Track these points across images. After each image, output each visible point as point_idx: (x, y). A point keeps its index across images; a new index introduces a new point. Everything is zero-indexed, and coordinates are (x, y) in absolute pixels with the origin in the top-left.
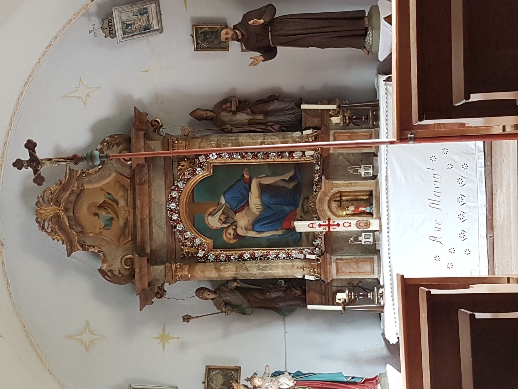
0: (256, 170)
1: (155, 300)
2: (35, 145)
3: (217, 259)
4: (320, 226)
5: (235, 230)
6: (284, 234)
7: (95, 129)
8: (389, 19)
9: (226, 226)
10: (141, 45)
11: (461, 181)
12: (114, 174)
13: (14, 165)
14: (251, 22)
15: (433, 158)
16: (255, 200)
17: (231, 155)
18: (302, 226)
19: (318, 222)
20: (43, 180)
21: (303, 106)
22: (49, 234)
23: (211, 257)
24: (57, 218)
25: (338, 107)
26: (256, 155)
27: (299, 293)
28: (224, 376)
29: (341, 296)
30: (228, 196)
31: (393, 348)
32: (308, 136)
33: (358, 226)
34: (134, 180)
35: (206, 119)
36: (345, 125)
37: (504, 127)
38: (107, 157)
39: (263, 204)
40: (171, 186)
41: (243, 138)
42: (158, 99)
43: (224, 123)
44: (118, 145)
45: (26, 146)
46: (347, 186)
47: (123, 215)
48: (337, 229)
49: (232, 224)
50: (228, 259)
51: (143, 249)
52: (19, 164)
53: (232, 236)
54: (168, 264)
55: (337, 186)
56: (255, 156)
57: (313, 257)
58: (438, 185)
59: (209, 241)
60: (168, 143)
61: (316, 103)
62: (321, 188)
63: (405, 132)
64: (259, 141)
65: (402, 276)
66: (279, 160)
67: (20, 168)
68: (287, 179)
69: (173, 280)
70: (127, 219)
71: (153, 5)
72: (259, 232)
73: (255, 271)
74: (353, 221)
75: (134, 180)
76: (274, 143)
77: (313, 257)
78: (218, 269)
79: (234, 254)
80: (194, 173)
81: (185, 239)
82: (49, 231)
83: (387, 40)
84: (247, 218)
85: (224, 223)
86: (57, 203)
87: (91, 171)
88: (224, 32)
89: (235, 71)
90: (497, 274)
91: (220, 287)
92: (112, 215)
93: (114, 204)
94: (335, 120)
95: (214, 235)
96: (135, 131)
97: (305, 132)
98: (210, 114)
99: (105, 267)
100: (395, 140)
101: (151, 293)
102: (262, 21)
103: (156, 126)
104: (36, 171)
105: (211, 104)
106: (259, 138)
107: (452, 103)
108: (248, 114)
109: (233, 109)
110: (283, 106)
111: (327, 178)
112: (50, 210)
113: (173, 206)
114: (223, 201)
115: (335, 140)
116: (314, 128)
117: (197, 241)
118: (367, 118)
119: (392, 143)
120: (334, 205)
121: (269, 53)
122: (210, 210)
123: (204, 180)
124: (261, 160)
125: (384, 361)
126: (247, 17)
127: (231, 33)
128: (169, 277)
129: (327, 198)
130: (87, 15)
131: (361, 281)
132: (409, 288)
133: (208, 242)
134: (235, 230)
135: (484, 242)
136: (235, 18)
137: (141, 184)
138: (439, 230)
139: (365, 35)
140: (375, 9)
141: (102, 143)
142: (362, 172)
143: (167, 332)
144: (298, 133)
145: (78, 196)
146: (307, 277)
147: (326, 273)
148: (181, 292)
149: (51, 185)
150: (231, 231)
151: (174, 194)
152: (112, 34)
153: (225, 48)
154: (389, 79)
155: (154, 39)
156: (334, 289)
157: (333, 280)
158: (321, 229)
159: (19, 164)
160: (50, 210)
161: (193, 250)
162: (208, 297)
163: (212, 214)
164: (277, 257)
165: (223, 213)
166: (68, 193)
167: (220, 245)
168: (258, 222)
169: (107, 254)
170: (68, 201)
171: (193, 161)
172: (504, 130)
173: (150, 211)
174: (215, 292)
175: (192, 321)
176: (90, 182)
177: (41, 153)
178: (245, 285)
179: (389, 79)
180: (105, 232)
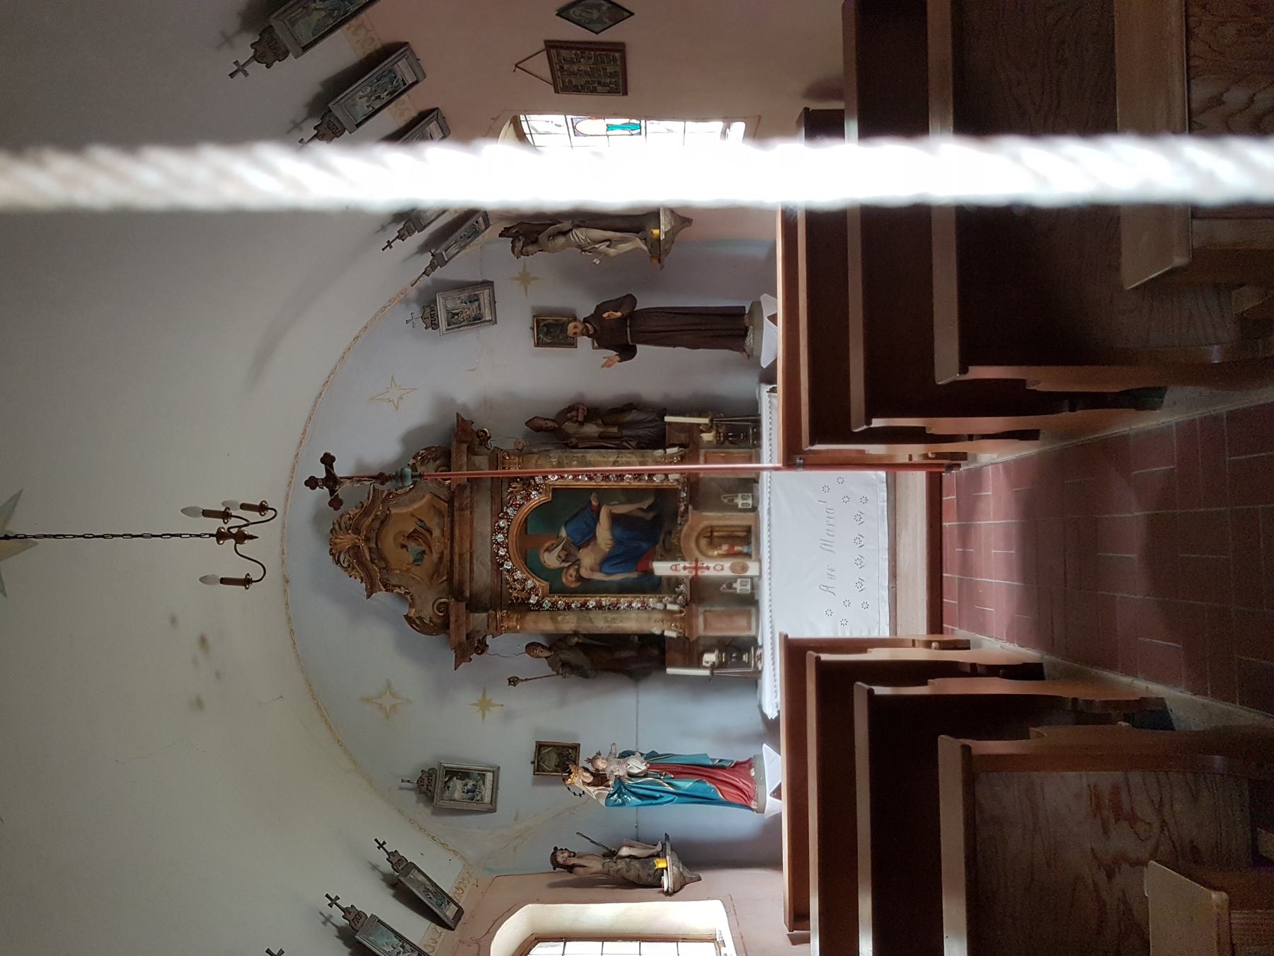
0: (606, 495)
1: (474, 656)
2: (333, 459)
3: (554, 604)
4: (685, 568)
5: (578, 571)
7: (407, 439)
8: (773, 318)
10: (469, 338)
11: (859, 518)
13: (307, 483)
14: (605, 315)
15: (826, 489)
16: (604, 533)
18: (662, 568)
19: (682, 564)
20: (341, 502)
21: (668, 419)
22: (346, 569)
23: (547, 604)
24: (355, 550)
25: (711, 421)
27: (656, 652)
28: (559, 755)
29: (710, 658)
31: (772, 726)
32: (672, 456)
33: (732, 569)
34: (453, 505)
35: (547, 430)
36: (719, 444)
38: (421, 476)
39: (614, 537)
40: (498, 513)
41: (592, 455)
42: (487, 403)
43: (569, 436)
44: (435, 460)
45: (323, 461)
46: (719, 518)
47: (437, 547)
49: (574, 564)
51: (462, 592)
52: (312, 483)
55: (708, 518)
56: (606, 478)
57: (676, 608)
59: (545, 584)
60: (496, 460)
61: (684, 415)
63: (793, 457)
64: (612, 459)
65: (786, 636)
66: (636, 484)
69: (497, 631)
70: (442, 553)
71: (487, 291)
72: (608, 574)
73: (601, 624)
74: (727, 564)
75: (453, 505)
77: (676, 608)
80: (527, 497)
83: (771, 342)
86: (357, 531)
87: (399, 492)
88: (571, 325)
89: (583, 372)
90: (901, 634)
91: (557, 643)
92: (424, 547)
93: (428, 535)
94: (707, 437)
95: (551, 576)
96: (456, 444)
97: (669, 451)
98: (550, 424)
99: (412, 613)
100: (780, 465)
101: (470, 648)
102: (619, 314)
103: (483, 438)
104: (332, 492)
105: (552, 412)
106: (612, 455)
107: (849, 429)
109: (580, 419)
110: (642, 416)
111: (695, 508)
112: (347, 540)
113: (500, 538)
114: (563, 533)
115: (706, 462)
116: (681, 446)
117: (530, 584)
118: (747, 436)
119: (776, 469)
120: (703, 542)
121: (627, 352)
122: (547, 545)
123: (540, 507)
124: (612, 483)
125: (759, 739)
126: (600, 309)
127: (580, 327)
128: (492, 629)
129: (695, 534)
130: (406, 302)
131: (734, 639)
132: (795, 652)
133: (542, 585)
134: (578, 571)
135: (885, 594)
136: (586, 308)
138: (831, 577)
139: (745, 335)
140: (757, 306)
141: (414, 458)
142: (740, 502)
143: (488, 698)
144: (660, 452)
145: (382, 522)
146: (667, 633)
147: (691, 627)
148: (508, 647)
149: (350, 509)
150: (572, 571)
152: (434, 325)
153: (573, 344)
154: (773, 390)
155: (485, 332)
156: (701, 648)
157: (699, 638)
158: (685, 573)
159: (312, 483)
160: (347, 540)
161: (524, 595)
163: (548, 550)
164: (630, 606)
165: (563, 549)
167: (557, 589)
168: (607, 562)
169: (416, 597)
170: (370, 529)
171: (527, 483)
172: (910, 458)
174: (550, 649)
175: (519, 684)
176: (397, 505)
177: (340, 470)
178: (589, 641)
179: (773, 390)
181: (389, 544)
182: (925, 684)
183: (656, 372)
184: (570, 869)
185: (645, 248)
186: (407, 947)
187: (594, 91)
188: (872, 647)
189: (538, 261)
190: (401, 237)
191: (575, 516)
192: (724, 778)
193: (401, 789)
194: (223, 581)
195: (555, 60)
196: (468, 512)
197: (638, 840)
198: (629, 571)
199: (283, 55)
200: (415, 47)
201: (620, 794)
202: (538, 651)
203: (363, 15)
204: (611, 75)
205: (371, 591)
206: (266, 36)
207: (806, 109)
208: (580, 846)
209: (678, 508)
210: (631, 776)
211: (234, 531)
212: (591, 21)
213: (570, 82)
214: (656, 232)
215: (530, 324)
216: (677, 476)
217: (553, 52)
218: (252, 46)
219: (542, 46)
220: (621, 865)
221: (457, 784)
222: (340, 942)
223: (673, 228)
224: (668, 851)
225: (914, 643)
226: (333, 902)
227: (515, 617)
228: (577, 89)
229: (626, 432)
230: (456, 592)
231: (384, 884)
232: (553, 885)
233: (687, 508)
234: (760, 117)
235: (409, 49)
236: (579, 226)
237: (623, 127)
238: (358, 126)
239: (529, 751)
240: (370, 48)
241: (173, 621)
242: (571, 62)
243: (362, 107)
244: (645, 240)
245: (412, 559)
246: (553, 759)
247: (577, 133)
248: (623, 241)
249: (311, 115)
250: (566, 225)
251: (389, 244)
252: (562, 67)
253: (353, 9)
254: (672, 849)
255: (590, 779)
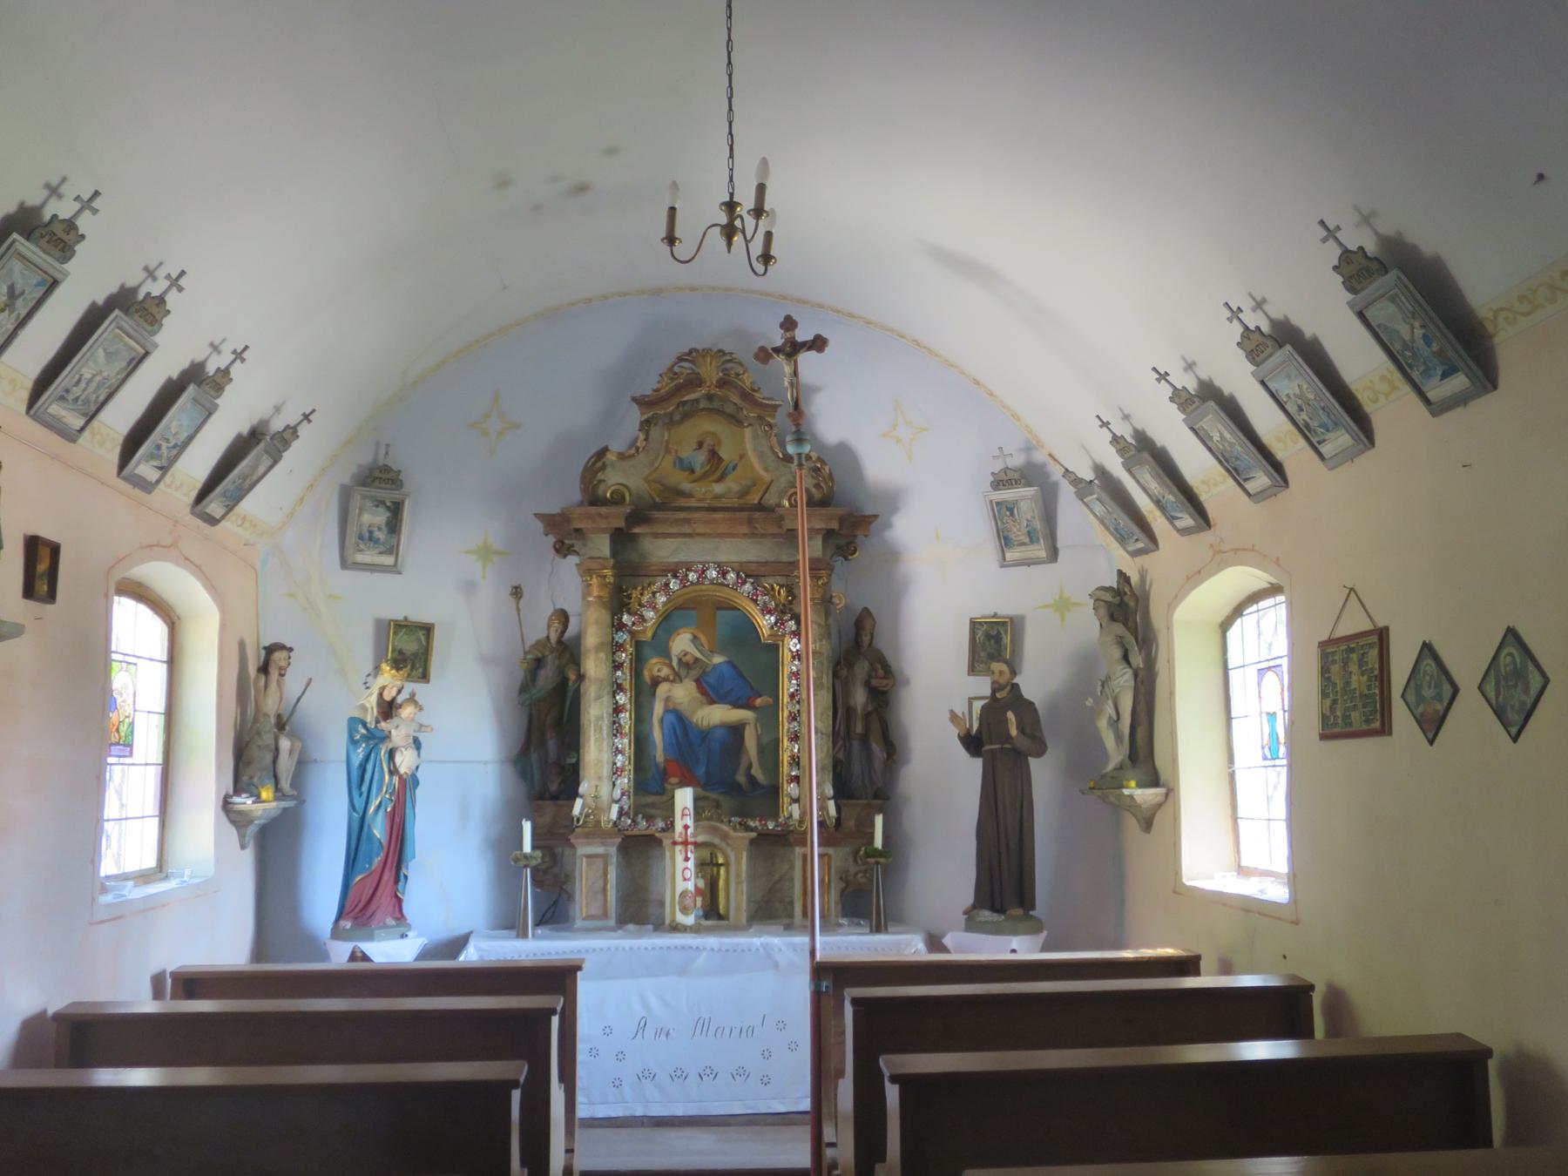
0: (769, 717)
1: (552, 539)
3: (620, 647)
4: (686, 827)
5: (666, 679)
6: (656, 765)
9: (675, 663)
10: (982, 530)
12: (767, 477)
16: (718, 715)
17: (796, 675)
18: (684, 798)
19: (689, 821)
22: (671, 369)
23: (622, 637)
24: (695, 382)
26: (794, 719)
27: (554, 787)
28: (416, 655)
30: (727, 670)
33: (684, 894)
37: (833, 1145)
40: (749, 572)
41: (826, 697)
42: (892, 556)
43: (850, 665)
46: (738, 876)
47: (699, 489)
48: (679, 858)
49: (676, 674)
50: (617, 666)
52: (789, 324)
53: (656, 673)
54: (612, 562)
56: (793, 717)
57: (614, 815)
58: (736, 1032)
59: (649, 634)
62: (735, 829)
65: (579, 968)
66: (785, 758)
67: (782, 326)
68: (753, 772)
69: (586, 572)
72: (662, 721)
73: (594, 710)
75: (755, 513)
76: (816, 751)
78: (599, 648)
79: (623, 676)
80: (766, 610)
81: (654, 593)
82: (676, 369)
84: (686, 700)
85: (680, 660)
86: (722, 383)
87: (774, 440)
88: (1004, 667)
89: (937, 690)
90: (577, 1131)
91: (568, 651)
92: (699, 471)
93: (718, 474)
97: (831, 805)
98: (866, 640)
99: (611, 457)
102: (1014, 732)
104: (777, 350)
105: (882, 644)
108: (865, 706)
109: (874, 682)
110: (878, 765)
111: (752, 842)
112: (710, 372)
114: (718, 659)
115: (821, 856)
116: (838, 820)
119: (813, 953)
122: (703, 638)
123: (753, 629)
124: (786, 727)
127: (1002, 680)
130: (1028, 448)
134: (666, 679)
137: (750, 522)
139: (994, 909)
141: (819, 459)
144: (830, 791)
146: (579, 803)
147: (588, 836)
148: (568, 588)
150: (665, 672)
151: (731, 576)
153: (972, 670)
157: (573, 847)
159: (789, 324)
160: (710, 372)
162: (553, 630)
163: (695, 639)
164: (618, 751)
165: (696, 660)
166: (737, 401)
168: (679, 722)
170: (726, 400)
171: (786, 610)
173: (703, 535)
174: (560, 641)
175: (512, 601)
176: (755, 437)
177: (806, 359)
180: (670, 458)
181: (706, 425)
182: (523, 1163)
183: (942, 787)
184: (264, 669)
185: (1110, 767)
186: (175, 452)
187: (1324, 695)
188: (566, 1091)
189: (1087, 625)
190: (1116, 440)
191: (741, 675)
192: (376, 883)
193: (377, 444)
194: (673, 210)
195: (1362, 642)
196: (745, 530)
197: (302, 764)
198: (665, 750)
199: (1352, 284)
200: (1370, 454)
201: (366, 738)
202: (556, 625)
203: (1406, 388)
204: (1346, 717)
205: (642, 402)
206: (1375, 266)
207: (1311, 987)
208: (293, 684)
209: (753, 818)
210: (391, 754)
211: (738, 223)
212: (1418, 688)
213: (1334, 662)
214: (1133, 784)
215: (1000, 613)
216: (796, 814)
217: (1375, 639)
218: (1361, 248)
219: (1381, 624)
220: (268, 739)
221: (380, 517)
222: (185, 364)
223: (1138, 806)
224: (284, 804)
225: (569, 1151)
226: (239, 356)
227: (605, 594)
228: (1325, 671)
229: (856, 744)
230: (640, 515)
231: (255, 422)
232: (242, 645)
233: (752, 830)
234: (1296, 923)
235: (1368, 449)
236: (1136, 675)
237: (1273, 735)
238: (1263, 383)
239: (420, 615)
240: (1364, 397)
241: (611, 151)
242: (1361, 663)
243: (1286, 388)
244: (1121, 767)
245: (684, 455)
246: (410, 645)
247: (1262, 672)
248: (1119, 738)
249: (1274, 323)
250: (1137, 659)
251: (1105, 424)
252: (1352, 650)
253: (1415, 375)
254: (285, 810)
255: (387, 697)
